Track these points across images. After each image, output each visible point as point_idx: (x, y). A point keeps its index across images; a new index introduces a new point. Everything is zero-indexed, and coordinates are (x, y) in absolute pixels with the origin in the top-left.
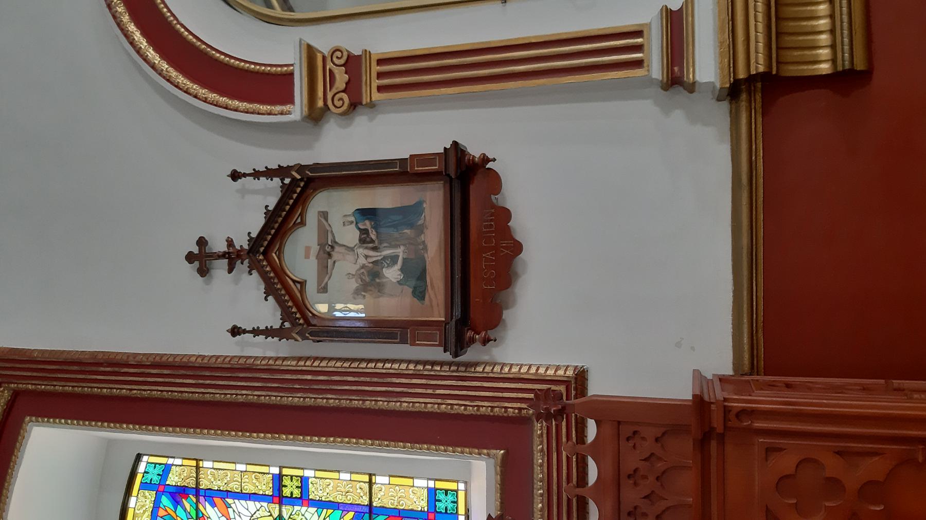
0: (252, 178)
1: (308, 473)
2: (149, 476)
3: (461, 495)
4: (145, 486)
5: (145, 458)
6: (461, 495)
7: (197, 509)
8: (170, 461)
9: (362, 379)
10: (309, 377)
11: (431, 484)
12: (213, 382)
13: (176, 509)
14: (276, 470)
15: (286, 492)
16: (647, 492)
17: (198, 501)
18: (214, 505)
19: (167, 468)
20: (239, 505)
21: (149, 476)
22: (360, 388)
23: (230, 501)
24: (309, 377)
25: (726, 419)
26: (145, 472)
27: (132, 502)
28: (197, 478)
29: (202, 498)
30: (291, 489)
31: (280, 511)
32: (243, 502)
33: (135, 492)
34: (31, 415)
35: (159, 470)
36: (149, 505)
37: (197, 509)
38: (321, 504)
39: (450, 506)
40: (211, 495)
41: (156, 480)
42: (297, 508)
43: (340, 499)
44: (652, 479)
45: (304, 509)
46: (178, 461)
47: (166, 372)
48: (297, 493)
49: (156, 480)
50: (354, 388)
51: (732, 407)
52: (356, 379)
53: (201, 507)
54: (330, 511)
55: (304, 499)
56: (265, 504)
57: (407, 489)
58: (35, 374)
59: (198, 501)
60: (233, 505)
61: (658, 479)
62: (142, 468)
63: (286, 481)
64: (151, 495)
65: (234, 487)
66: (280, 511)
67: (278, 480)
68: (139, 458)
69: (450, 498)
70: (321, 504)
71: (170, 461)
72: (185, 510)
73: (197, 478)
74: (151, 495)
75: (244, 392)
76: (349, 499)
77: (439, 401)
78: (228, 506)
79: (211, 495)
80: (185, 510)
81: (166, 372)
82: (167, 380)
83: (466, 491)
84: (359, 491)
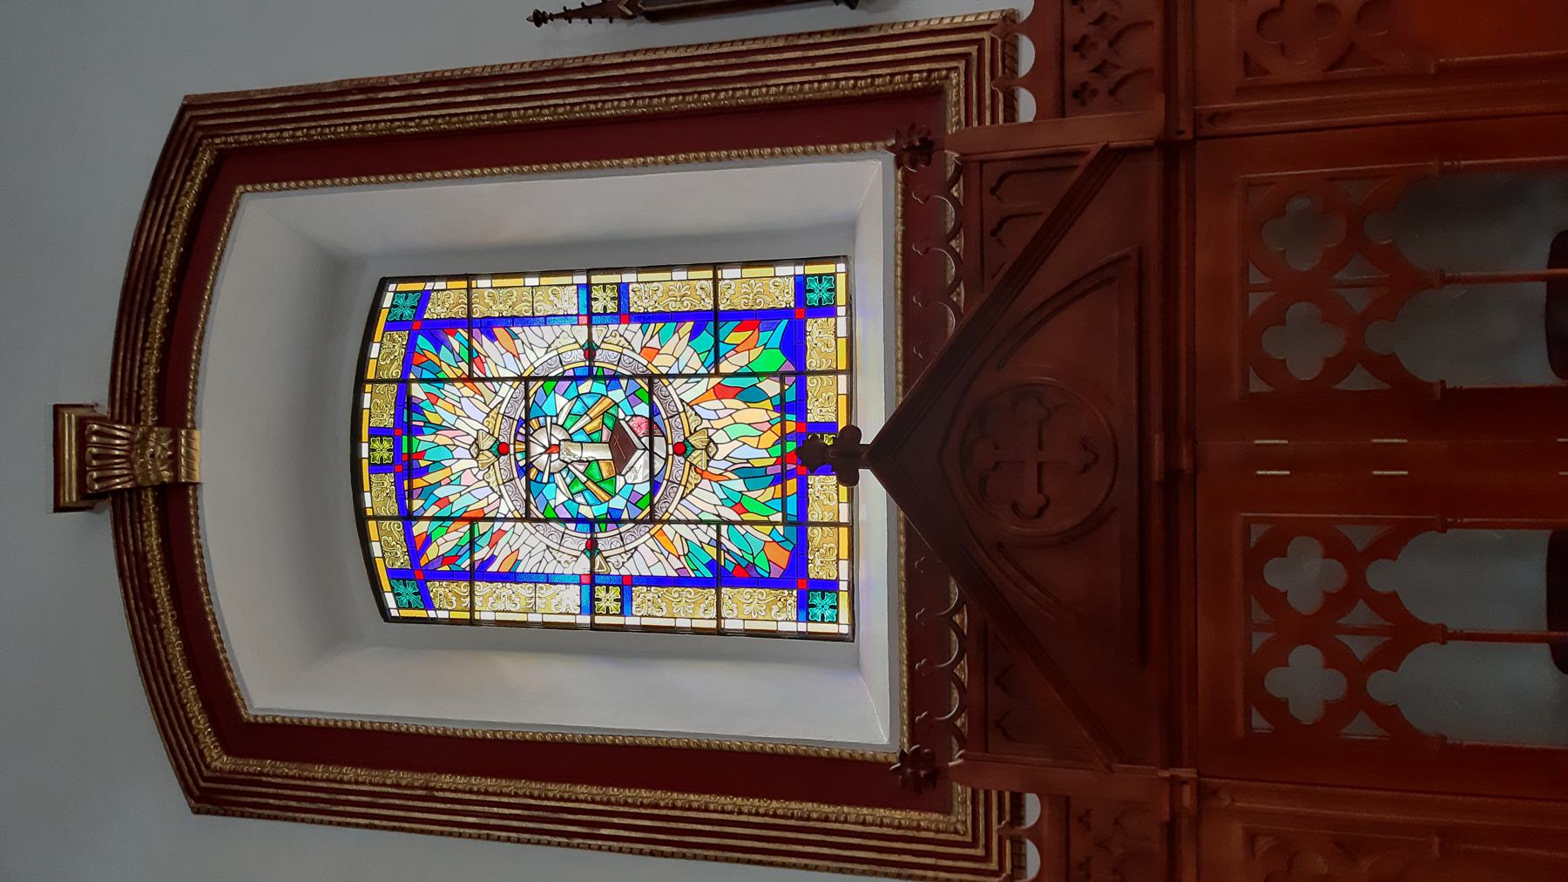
3: (841, 279)
6: (841, 279)
7: (470, 349)
9: (715, 62)
10: (642, 70)
11: (799, 270)
12: (509, 94)
16: (1096, 16)
17: (471, 336)
18: (493, 338)
19: (425, 296)
21: (377, 455)
22: (712, 75)
23: (517, 330)
24: (642, 70)
25: (1196, 125)
26: (393, 306)
27: (375, 350)
28: (469, 304)
29: (476, 331)
31: (590, 335)
32: (535, 329)
33: (378, 337)
34: (244, 183)
35: (413, 301)
36: (399, 351)
37: (470, 349)
38: (645, 318)
39: (826, 295)
40: (487, 326)
41: (408, 314)
42: (612, 327)
43: (673, 307)
44: (1103, 45)
45: (623, 327)
47: (442, 89)
48: (612, 307)
49: (408, 314)
50: (704, 76)
52: (707, 63)
53: (475, 344)
54: (659, 325)
56: (567, 328)
57: (765, 281)
58: (252, 119)
59: (471, 336)
60: (522, 336)
61: (1111, 44)
62: (387, 302)
64: (401, 337)
65: (523, 309)
66: (590, 335)
68: (383, 284)
70: (645, 318)
71: (429, 286)
72: (452, 351)
73: (469, 304)
75: (552, 102)
76: (686, 306)
77: (820, 77)
78: (514, 337)
79: (487, 326)
80: (452, 351)
81: (442, 89)
82: (443, 100)
83: (847, 273)
84: (663, 605)
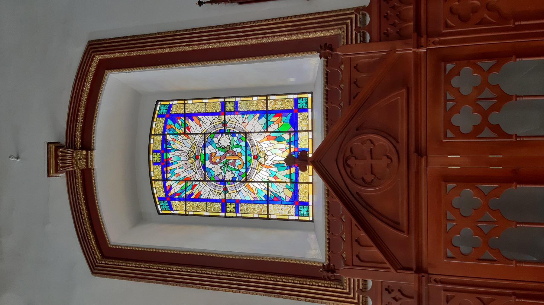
0: (210, 4)
1: (237, 99)
2: (306, 209)
3: (310, 99)
4: (159, 116)
5: (159, 103)
7: (185, 123)
8: (171, 103)
13: (175, 124)
14: (222, 100)
15: (233, 205)
18: (192, 120)
20: (205, 118)
23: (200, 117)
30: (230, 107)
32: (207, 117)
37: (185, 123)
38: (244, 113)
39: (162, 204)
40: (191, 116)
41: (165, 111)
45: (236, 116)
46: (175, 102)
48: (228, 205)
51: (420, 52)
53: (186, 121)
54: (248, 115)
55: (236, 111)
60: (202, 119)
63: (233, 210)
64: (162, 120)
67: (223, 105)
69: (163, 207)
71: (171, 103)
74: (162, 120)
78: (200, 120)
79: (191, 116)
80: (179, 124)
